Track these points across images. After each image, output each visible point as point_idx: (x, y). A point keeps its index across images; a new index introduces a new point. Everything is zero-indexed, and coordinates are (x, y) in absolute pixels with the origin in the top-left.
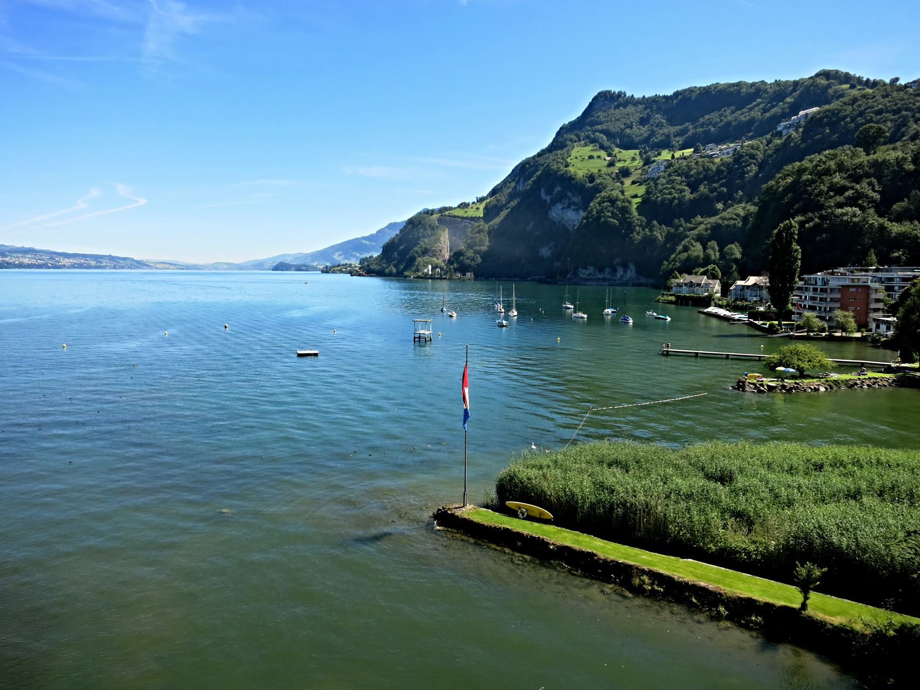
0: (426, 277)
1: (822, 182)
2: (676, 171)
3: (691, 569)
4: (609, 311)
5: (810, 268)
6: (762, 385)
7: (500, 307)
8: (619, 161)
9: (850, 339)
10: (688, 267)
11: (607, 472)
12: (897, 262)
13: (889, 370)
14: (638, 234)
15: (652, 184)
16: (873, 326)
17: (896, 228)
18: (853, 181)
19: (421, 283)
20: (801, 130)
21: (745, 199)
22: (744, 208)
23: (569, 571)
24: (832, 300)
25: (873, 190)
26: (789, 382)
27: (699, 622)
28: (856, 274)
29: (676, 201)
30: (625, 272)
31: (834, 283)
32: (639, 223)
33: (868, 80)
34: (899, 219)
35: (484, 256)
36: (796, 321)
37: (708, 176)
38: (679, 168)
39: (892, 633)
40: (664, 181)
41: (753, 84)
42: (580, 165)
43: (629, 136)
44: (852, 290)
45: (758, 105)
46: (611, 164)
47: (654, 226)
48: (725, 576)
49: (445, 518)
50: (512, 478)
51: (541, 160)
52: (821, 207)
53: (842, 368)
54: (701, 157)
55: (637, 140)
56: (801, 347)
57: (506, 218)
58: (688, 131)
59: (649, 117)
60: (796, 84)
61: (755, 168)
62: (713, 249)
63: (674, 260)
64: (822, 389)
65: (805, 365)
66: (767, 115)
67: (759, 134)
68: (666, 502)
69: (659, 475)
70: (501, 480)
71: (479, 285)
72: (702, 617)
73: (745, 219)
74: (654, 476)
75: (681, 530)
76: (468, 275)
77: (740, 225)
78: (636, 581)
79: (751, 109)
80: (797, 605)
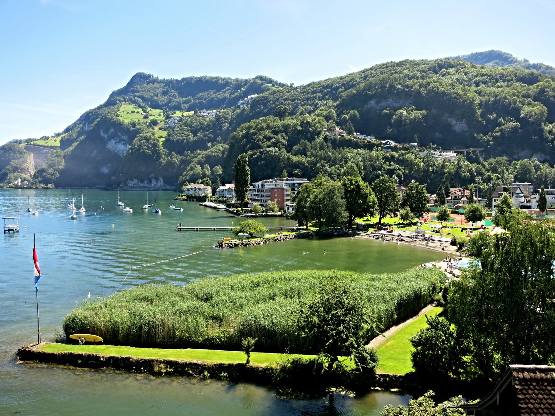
0: (16, 187)
1: (260, 134)
2: (184, 124)
3: (189, 354)
4: (146, 206)
5: (255, 179)
6: (231, 244)
7: (72, 206)
8: (151, 115)
9: (276, 216)
10: (193, 180)
11: (138, 305)
12: (296, 176)
13: (293, 230)
14: (164, 159)
15: (171, 130)
16: (286, 208)
17: (295, 159)
18: (274, 134)
19: (12, 191)
20: (249, 106)
21: (223, 141)
22: (222, 146)
23: (48, 367)
24: (267, 196)
25: (284, 139)
26: (245, 241)
27: (194, 384)
28: (278, 182)
29: (185, 141)
30: (157, 182)
31: (267, 187)
32: (164, 153)
33: (280, 83)
34: (296, 154)
35: (61, 172)
36: (250, 207)
37: (204, 128)
38: (186, 122)
39: (289, 365)
40: (178, 129)
41: (224, 79)
42: (126, 116)
43: (156, 101)
44: (276, 190)
45: (228, 90)
46: (146, 117)
47: (173, 155)
48: (208, 354)
49: (25, 355)
50: (73, 320)
51: (100, 112)
52: (260, 147)
53: (271, 231)
54: (198, 117)
55: (161, 104)
56: (251, 221)
57: (77, 147)
58: (191, 101)
59: (168, 91)
60: (246, 81)
61: (227, 125)
62: (207, 169)
63: (186, 175)
64: (262, 243)
65: (253, 231)
66: (233, 96)
67: (229, 106)
68: (173, 317)
69: (170, 302)
70: (66, 321)
71: (58, 192)
72: (195, 381)
73: (223, 152)
74: (167, 304)
75: (183, 332)
76: (50, 185)
77: (221, 155)
78: (157, 369)
79: (224, 92)
80: (244, 362)
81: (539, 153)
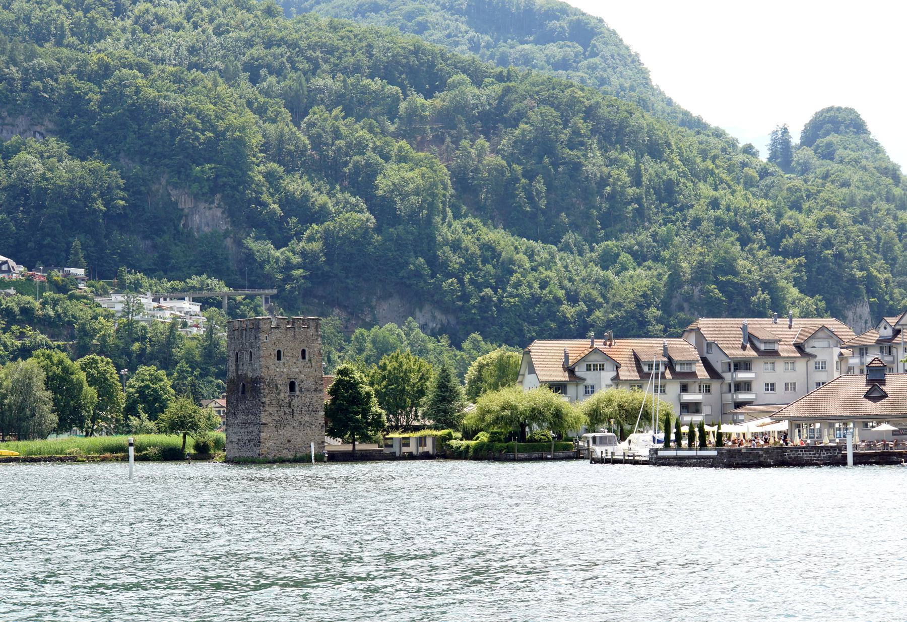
81: (427, 307)
